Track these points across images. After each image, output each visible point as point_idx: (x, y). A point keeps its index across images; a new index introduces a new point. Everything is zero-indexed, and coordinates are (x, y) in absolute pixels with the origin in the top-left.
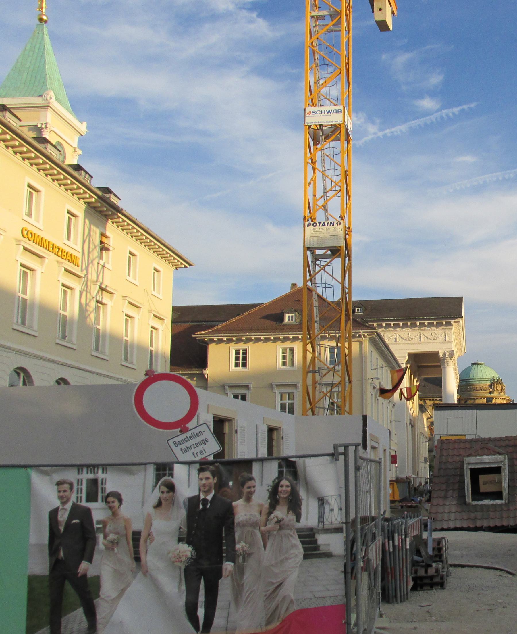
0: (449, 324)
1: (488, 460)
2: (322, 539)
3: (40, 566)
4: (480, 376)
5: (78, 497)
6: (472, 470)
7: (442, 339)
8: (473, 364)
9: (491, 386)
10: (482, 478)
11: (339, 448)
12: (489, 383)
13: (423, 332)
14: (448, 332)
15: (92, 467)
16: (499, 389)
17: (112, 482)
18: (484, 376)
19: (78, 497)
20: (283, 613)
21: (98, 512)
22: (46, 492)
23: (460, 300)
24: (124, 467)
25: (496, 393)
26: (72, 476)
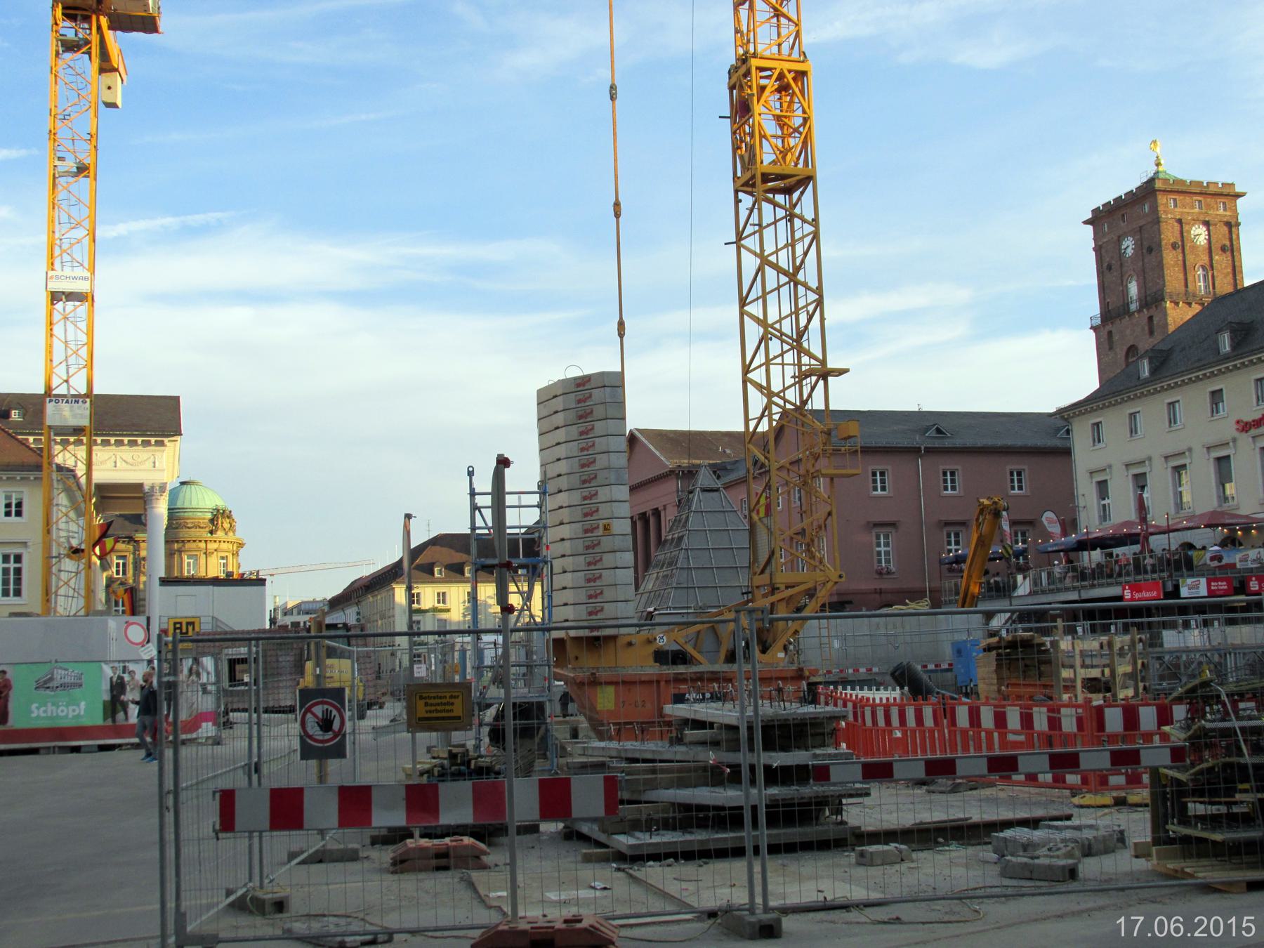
0: (161, 444)
1: (242, 651)
2: (209, 688)
3: (107, 697)
4: (194, 504)
5: (119, 672)
6: (230, 661)
7: (149, 465)
8: (183, 483)
9: (212, 521)
10: (238, 667)
11: (424, 667)
12: (209, 516)
13: (119, 454)
14: (158, 455)
15: (124, 661)
16: (227, 525)
17: (131, 667)
18: (201, 505)
19: (119, 672)
20: (194, 713)
21: (127, 677)
22: (108, 671)
23: (177, 399)
24: (136, 661)
25: (220, 534)
26: (116, 665)
